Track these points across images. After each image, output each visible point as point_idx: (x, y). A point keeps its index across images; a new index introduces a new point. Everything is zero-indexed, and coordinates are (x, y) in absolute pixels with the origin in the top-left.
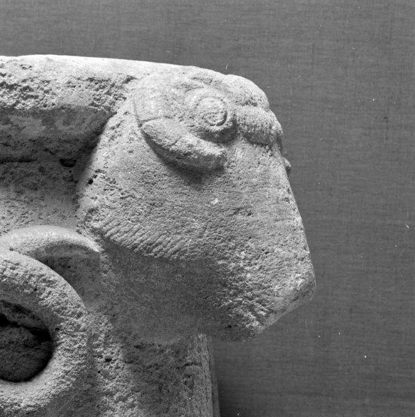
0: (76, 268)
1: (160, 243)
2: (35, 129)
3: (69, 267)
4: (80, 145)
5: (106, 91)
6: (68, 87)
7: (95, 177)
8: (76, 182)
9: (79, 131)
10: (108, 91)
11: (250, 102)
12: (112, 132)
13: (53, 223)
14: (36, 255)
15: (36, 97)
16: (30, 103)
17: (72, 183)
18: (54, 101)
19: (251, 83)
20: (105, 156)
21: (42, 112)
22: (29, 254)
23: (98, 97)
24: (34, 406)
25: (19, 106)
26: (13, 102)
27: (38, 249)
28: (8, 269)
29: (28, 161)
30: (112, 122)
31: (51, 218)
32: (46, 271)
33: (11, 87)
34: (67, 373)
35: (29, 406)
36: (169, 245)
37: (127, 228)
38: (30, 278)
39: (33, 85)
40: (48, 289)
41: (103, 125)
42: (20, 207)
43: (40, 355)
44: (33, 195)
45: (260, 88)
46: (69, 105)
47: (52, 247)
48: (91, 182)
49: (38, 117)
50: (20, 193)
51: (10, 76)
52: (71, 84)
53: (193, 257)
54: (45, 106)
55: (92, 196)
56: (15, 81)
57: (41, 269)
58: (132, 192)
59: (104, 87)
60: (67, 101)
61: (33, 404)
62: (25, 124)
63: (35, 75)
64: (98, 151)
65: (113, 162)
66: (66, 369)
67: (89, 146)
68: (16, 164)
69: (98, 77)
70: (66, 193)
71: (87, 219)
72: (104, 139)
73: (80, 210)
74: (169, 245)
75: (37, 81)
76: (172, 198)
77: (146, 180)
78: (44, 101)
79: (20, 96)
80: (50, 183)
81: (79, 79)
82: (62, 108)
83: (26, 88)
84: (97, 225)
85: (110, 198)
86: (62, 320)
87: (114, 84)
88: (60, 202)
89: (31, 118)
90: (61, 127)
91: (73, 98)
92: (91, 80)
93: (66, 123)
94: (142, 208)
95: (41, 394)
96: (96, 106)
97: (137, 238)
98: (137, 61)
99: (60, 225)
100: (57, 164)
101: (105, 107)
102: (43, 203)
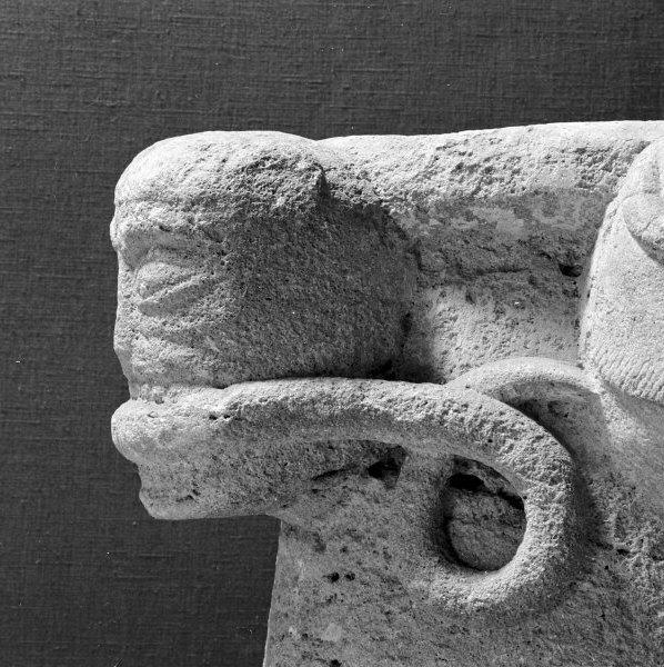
0: (574, 416)
1: (644, 375)
2: (515, 227)
3: (566, 416)
5: (603, 165)
6: (547, 163)
10: (607, 165)
13: (545, 355)
14: (502, 396)
16: (495, 188)
18: (524, 184)
20: (601, 263)
21: (509, 199)
22: (489, 393)
23: (590, 175)
24: (486, 601)
25: (481, 194)
27: (502, 387)
28: (451, 412)
31: (544, 347)
32: (511, 415)
33: (472, 169)
34: (533, 558)
38: (481, 425)
39: (498, 165)
40: (510, 441)
42: (498, 331)
44: (520, 315)
45: (589, 120)
46: (545, 188)
47: (520, 385)
49: (507, 207)
50: (499, 312)
51: (470, 155)
52: (551, 160)
54: (513, 192)
56: (475, 161)
57: (501, 414)
59: (602, 159)
60: (544, 183)
61: (483, 598)
62: (494, 218)
63: (504, 150)
66: (532, 553)
68: (498, 275)
69: (592, 146)
78: (511, 185)
79: (482, 180)
80: (543, 298)
81: (563, 151)
82: (536, 193)
83: (488, 170)
86: (529, 485)
87: (617, 154)
88: (555, 325)
89: (497, 209)
90: (545, 220)
91: (551, 178)
92: (582, 151)
93: (547, 213)
95: (496, 586)
96: (586, 187)
98: (650, 123)
99: (555, 356)
100: (556, 273)
101: (601, 187)
102: (532, 327)
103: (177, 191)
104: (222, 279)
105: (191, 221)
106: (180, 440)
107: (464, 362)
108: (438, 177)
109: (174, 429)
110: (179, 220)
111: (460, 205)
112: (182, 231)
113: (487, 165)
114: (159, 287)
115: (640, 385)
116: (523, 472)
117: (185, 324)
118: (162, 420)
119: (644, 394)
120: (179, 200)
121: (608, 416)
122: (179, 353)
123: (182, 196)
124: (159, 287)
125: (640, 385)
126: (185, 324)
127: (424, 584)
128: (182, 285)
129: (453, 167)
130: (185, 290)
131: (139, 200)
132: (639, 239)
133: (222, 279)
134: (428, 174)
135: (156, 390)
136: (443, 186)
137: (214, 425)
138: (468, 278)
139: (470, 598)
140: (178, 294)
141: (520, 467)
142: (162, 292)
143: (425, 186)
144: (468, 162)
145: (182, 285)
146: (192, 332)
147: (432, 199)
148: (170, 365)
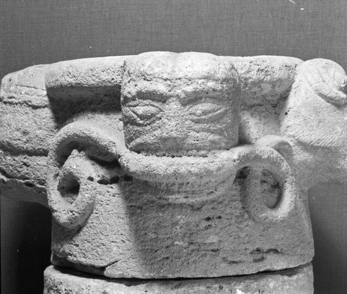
4: (278, 97)
7: (289, 111)
8: (279, 114)
9: (279, 90)
11: (236, 61)
12: (295, 90)
15: (270, 75)
16: (269, 77)
17: (277, 115)
19: (330, 60)
20: (293, 102)
25: (265, 79)
26: (263, 77)
29: (262, 105)
30: (294, 86)
34: (292, 201)
35: (282, 217)
36: (327, 140)
37: (307, 134)
41: (290, 87)
43: (276, 195)
48: (286, 114)
53: (338, 144)
55: (288, 121)
58: (309, 117)
64: (289, 99)
65: (299, 104)
67: (284, 97)
70: (275, 120)
71: (286, 131)
72: (292, 94)
73: (282, 127)
74: (327, 140)
75: (270, 67)
76: (328, 118)
77: (317, 111)
83: (267, 71)
84: (291, 133)
85: (298, 120)
86: (288, 177)
94: (315, 123)
97: (313, 138)
103: (218, 76)
104: (230, 109)
105: (223, 87)
106: (224, 170)
107: (255, 137)
108: (252, 73)
109: (223, 166)
110: (219, 87)
111: (258, 83)
112: (221, 91)
113: (266, 69)
114: (210, 112)
115: (321, 143)
116: (287, 173)
117: (218, 126)
118: (218, 163)
119: (323, 145)
120: (220, 79)
121: (295, 153)
122: (216, 137)
123: (221, 78)
124: (210, 112)
125: (321, 143)
126: (218, 126)
127: (265, 214)
128: (219, 112)
129: (257, 70)
130: (220, 113)
131: (200, 79)
132: (321, 95)
133: (230, 109)
134: (248, 72)
135: (203, 152)
136: (254, 76)
137: (235, 163)
138: (251, 108)
139: (279, 217)
140: (217, 115)
141: (286, 172)
142: (211, 114)
143: (248, 76)
144: (262, 67)
145: (219, 112)
146: (221, 130)
147: (250, 80)
148: (213, 142)
